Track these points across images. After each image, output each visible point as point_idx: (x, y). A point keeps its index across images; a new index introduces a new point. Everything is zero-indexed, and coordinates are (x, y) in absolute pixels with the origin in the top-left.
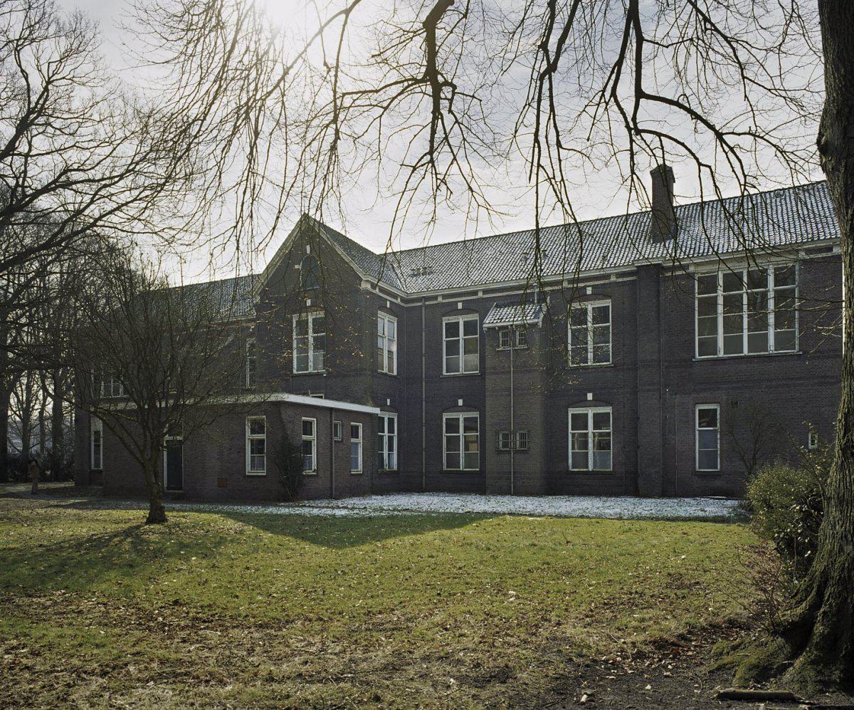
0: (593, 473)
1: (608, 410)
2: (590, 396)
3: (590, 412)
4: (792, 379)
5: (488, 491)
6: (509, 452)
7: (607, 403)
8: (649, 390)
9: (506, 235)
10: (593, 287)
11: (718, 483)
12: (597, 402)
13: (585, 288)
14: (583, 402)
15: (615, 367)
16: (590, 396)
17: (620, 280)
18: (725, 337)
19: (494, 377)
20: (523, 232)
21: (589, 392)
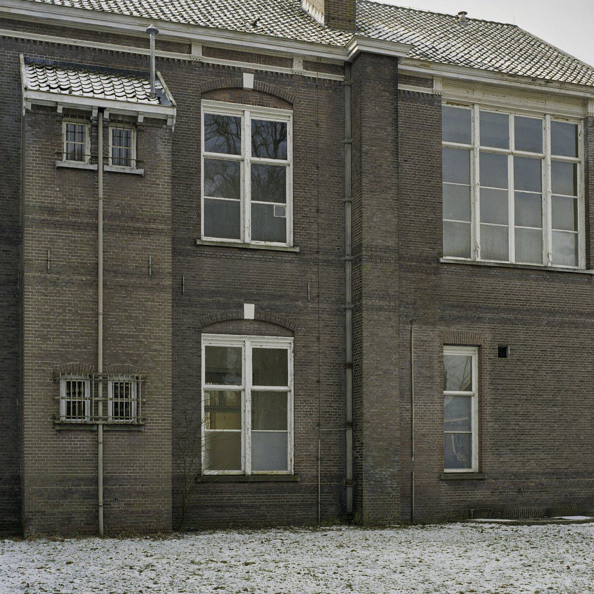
0: (255, 480)
1: (284, 343)
2: (249, 311)
3: (248, 345)
4: (581, 314)
5: (32, 529)
6: (90, 428)
7: (285, 329)
8: (381, 309)
9: (486, 22)
10: (258, 74)
11: (480, 495)
12: (266, 323)
13: (240, 71)
14: (232, 322)
15: (299, 255)
16: (249, 311)
17: (312, 74)
18: (516, 229)
19: (48, 232)
20: (492, 23)
21: (249, 301)
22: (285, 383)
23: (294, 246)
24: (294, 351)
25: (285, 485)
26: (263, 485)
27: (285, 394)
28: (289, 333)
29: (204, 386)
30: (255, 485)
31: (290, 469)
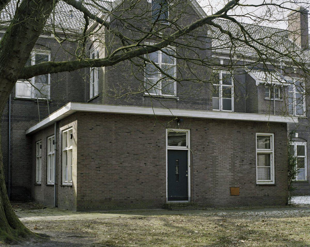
1: (304, 144)
2: (297, 135)
12: (301, 138)
13: (219, 60)
16: (297, 135)
22: (304, 155)
23: (177, 96)
24: (307, 146)
25: (306, 184)
26: (300, 184)
27: (304, 158)
28: (305, 141)
29: (189, 149)
30: (298, 184)
31: (306, 179)
